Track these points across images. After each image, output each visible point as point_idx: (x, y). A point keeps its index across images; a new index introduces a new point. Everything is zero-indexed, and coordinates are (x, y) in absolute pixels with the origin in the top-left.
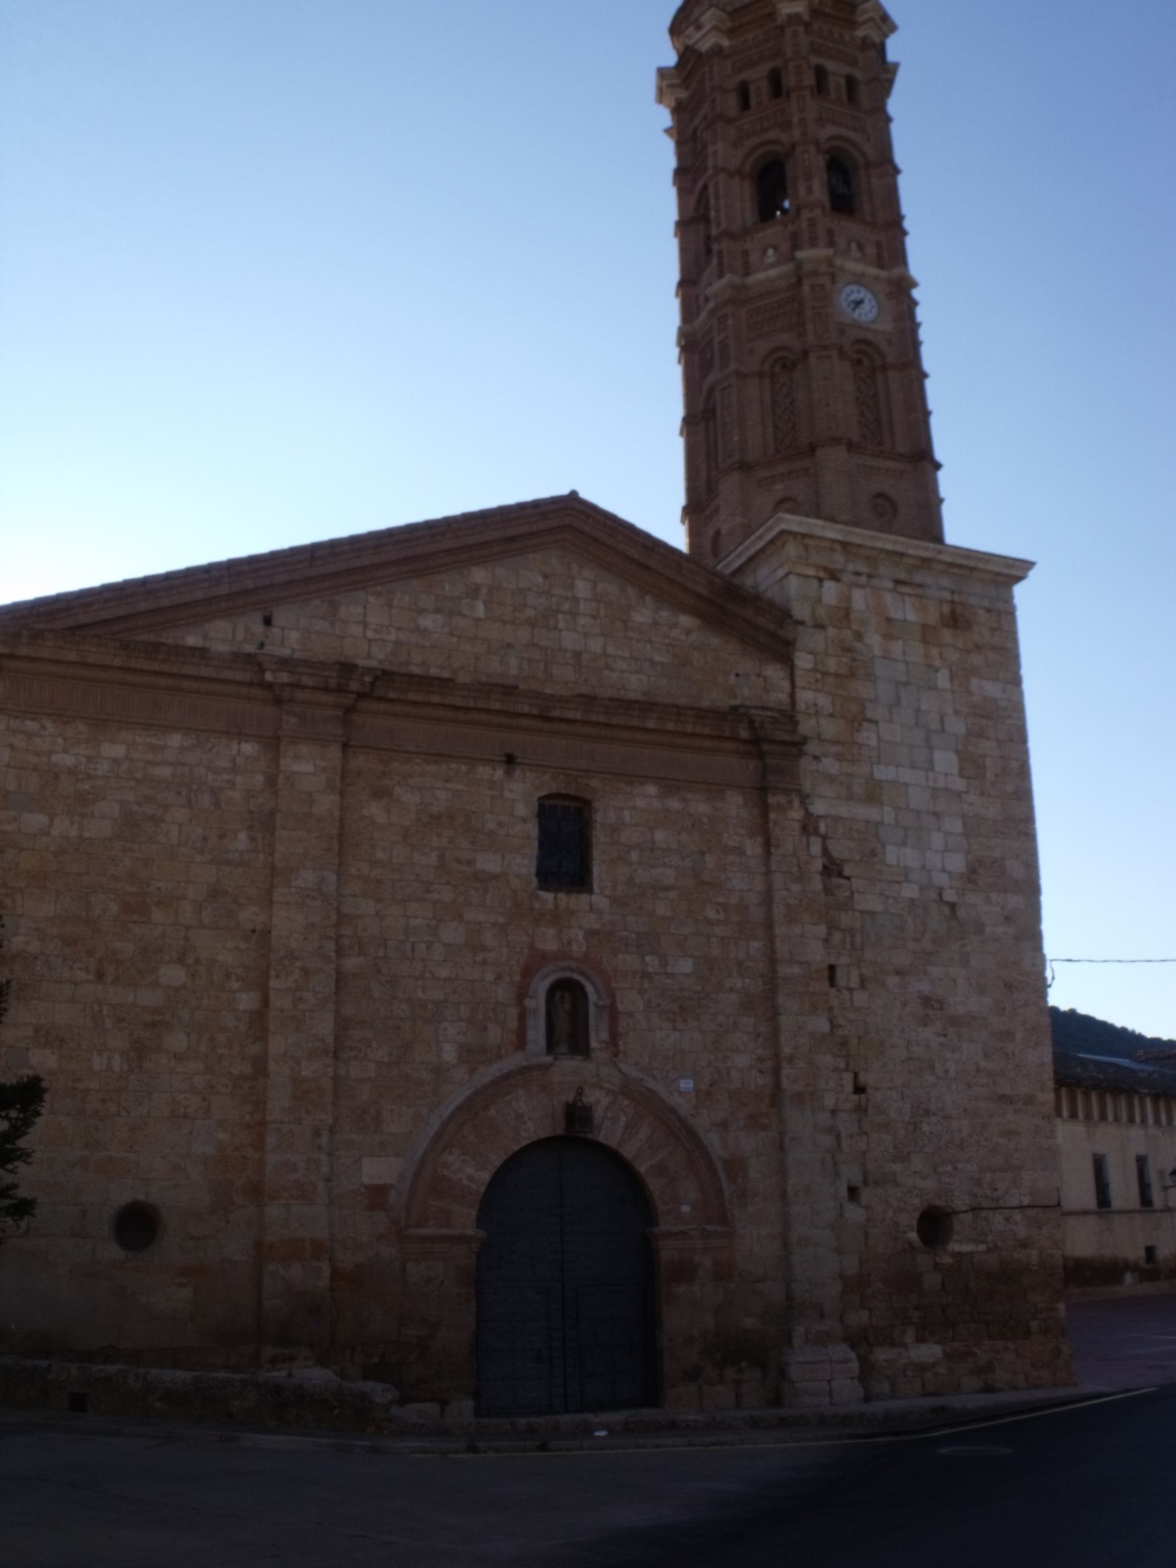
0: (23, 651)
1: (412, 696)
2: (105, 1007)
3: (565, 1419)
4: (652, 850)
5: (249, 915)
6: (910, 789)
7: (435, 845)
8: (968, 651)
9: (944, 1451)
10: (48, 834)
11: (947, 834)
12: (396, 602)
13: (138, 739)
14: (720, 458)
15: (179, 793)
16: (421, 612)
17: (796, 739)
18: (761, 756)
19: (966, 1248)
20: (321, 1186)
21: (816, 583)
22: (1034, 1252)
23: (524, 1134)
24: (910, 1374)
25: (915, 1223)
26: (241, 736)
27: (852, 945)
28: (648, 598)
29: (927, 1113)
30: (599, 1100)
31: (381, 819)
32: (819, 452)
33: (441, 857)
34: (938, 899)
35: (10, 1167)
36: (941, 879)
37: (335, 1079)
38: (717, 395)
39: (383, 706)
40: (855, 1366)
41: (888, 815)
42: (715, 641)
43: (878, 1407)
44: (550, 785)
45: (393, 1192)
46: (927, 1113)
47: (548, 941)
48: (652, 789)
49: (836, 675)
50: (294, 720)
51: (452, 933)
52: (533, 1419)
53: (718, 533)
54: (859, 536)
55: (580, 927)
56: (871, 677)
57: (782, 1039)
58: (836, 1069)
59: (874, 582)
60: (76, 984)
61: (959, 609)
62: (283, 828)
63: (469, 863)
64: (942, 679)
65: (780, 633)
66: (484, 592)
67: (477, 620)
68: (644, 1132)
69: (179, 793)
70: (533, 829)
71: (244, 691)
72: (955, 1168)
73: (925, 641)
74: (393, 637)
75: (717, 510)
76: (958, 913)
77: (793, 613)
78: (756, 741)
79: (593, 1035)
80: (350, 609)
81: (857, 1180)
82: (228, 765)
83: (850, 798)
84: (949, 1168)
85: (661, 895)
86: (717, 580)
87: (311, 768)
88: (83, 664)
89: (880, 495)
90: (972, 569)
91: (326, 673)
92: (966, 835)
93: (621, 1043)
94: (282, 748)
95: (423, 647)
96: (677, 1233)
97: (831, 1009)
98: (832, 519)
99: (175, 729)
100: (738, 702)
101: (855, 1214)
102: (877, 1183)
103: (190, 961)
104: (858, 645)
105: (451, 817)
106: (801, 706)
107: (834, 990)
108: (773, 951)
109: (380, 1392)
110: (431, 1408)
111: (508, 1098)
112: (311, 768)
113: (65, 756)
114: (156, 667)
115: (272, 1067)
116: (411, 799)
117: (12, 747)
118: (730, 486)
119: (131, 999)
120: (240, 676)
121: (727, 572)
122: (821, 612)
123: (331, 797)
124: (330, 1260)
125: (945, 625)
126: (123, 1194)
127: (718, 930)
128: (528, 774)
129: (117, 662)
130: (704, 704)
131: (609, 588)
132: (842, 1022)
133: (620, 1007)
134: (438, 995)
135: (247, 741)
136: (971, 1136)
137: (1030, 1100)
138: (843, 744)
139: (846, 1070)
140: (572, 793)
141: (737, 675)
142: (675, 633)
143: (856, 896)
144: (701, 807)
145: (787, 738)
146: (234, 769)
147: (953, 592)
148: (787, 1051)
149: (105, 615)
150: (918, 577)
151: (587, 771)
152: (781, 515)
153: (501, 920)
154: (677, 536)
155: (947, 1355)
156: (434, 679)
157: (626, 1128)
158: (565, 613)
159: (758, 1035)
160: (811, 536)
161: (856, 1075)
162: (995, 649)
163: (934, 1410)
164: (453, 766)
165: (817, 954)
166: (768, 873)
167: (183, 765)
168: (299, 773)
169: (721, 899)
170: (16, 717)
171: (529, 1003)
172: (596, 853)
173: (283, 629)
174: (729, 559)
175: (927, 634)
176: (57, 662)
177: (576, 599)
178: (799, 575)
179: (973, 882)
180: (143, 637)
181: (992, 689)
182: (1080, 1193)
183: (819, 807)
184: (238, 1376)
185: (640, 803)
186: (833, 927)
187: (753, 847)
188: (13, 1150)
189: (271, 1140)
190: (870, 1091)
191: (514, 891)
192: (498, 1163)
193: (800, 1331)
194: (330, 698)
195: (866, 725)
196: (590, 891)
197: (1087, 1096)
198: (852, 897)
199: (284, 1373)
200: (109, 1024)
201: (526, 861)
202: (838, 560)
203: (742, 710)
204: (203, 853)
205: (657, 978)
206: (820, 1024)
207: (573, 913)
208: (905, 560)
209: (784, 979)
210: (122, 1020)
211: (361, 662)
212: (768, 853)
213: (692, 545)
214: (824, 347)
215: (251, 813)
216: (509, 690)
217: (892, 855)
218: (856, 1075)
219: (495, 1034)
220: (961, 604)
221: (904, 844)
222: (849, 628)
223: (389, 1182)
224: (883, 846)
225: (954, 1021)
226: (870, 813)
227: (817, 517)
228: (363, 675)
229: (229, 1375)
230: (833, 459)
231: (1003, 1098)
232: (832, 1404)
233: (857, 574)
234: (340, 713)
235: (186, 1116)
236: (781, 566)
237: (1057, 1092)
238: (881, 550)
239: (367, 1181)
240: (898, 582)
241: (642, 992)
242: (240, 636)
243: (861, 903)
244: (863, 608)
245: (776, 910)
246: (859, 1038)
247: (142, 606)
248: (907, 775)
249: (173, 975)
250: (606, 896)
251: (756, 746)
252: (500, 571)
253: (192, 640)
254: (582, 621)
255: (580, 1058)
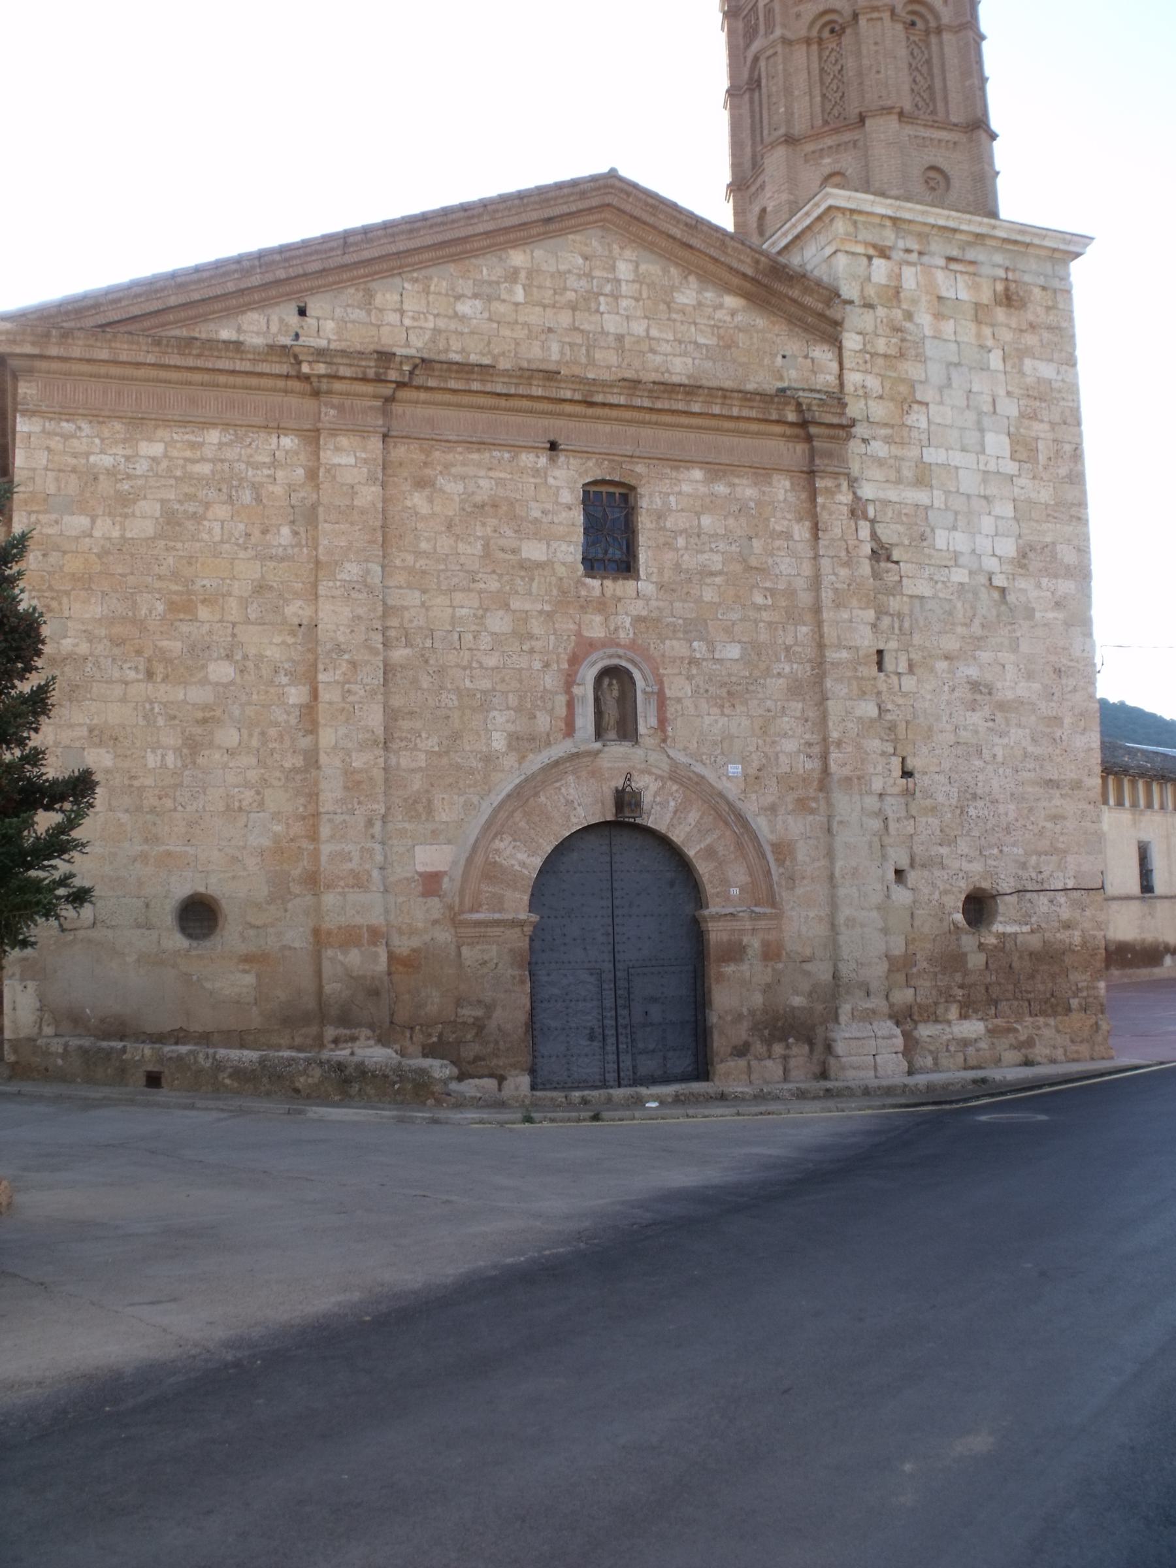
0: (54, 351)
1: (452, 384)
2: (156, 705)
3: (619, 1093)
4: (699, 536)
5: (295, 610)
6: (961, 472)
7: (479, 534)
8: (1022, 331)
9: (983, 1118)
10: (91, 536)
11: (997, 517)
12: (432, 288)
13: (175, 436)
14: (765, 132)
15: (220, 490)
16: (458, 297)
17: (844, 422)
18: (809, 439)
19: (1010, 929)
20: (375, 873)
21: (865, 260)
22: (1077, 933)
23: (574, 820)
24: (952, 1049)
25: (960, 905)
26: (280, 430)
27: (900, 629)
28: (692, 278)
29: (975, 796)
30: (648, 786)
31: (425, 509)
32: (868, 122)
33: (486, 546)
34: (987, 583)
35: (66, 857)
36: (991, 564)
37: (386, 769)
38: (762, 63)
39: (423, 396)
40: (899, 1042)
41: (939, 499)
42: (761, 322)
43: (921, 1079)
44: (595, 471)
45: (446, 879)
46: (975, 796)
47: (595, 629)
48: (697, 474)
49: (886, 356)
50: (332, 412)
51: (499, 622)
52: (586, 1093)
53: (764, 210)
54: (910, 211)
55: (626, 613)
56: (921, 358)
57: (830, 724)
58: (883, 754)
59: (925, 259)
60: (126, 683)
61: (1013, 286)
62: (326, 521)
63: (514, 552)
64: (995, 360)
65: (828, 313)
66: (523, 275)
67: (517, 304)
68: (693, 816)
69: (220, 490)
70: (578, 516)
71: (281, 384)
72: (1001, 851)
73: (978, 321)
74: (431, 325)
75: (762, 187)
76: (1008, 597)
77: (841, 292)
78: (804, 424)
79: (641, 721)
80: (386, 296)
81: (904, 863)
82: (267, 460)
83: (899, 481)
84: (995, 851)
85: (708, 581)
86: (763, 259)
87: (352, 461)
88: (116, 362)
89: (932, 168)
90: (1028, 245)
91: (363, 363)
92: (1015, 518)
93: (669, 729)
94: (322, 442)
95: (462, 334)
96: (726, 915)
97: (879, 693)
98: (883, 194)
99: (214, 425)
100: (786, 385)
101: (901, 895)
102: (923, 866)
103: (238, 657)
104: (908, 325)
105: (495, 506)
106: (849, 388)
107: (882, 674)
108: (821, 636)
109: (439, 1069)
110: (490, 1083)
111: (558, 785)
112: (352, 461)
113: (103, 456)
114: (190, 362)
115: (323, 759)
116: (454, 488)
117: (48, 449)
118: (776, 160)
119: (181, 697)
120: (277, 369)
121: (774, 250)
122: (871, 291)
123: (373, 489)
124: (387, 945)
125: (998, 303)
126: (182, 888)
127: (765, 615)
128: (572, 461)
129: (151, 359)
130: (750, 387)
131: (652, 268)
132: (889, 707)
133: (668, 693)
134: (486, 684)
135: (286, 435)
136: (1017, 820)
137: (1077, 785)
138: (892, 426)
139: (894, 754)
140: (617, 479)
141: (784, 357)
142: (719, 314)
143: (905, 580)
144: (748, 491)
145: (836, 420)
146: (274, 464)
147: (1007, 269)
148: (835, 735)
149: (136, 311)
150: (971, 255)
151: (632, 457)
152: (829, 190)
153: (547, 608)
154: (722, 215)
155: (990, 1031)
156: (474, 365)
157: (675, 812)
158: (606, 295)
159: (807, 721)
160: (860, 212)
161: (903, 759)
162: (1050, 328)
163: (975, 1082)
164: (496, 454)
165: (866, 641)
166: (816, 557)
167: (222, 461)
168: (340, 465)
169: (768, 584)
170: (51, 419)
171: (576, 690)
172: (642, 539)
173: (318, 319)
174: (774, 237)
175: (980, 313)
176: (89, 361)
177: (618, 281)
178: (847, 252)
179: (1023, 566)
180: (177, 332)
181: (1047, 371)
182: (1125, 878)
183: (867, 491)
184: (302, 1055)
185: (686, 488)
186: (881, 612)
187: (802, 532)
188: (68, 841)
189: (325, 831)
190: (917, 775)
191: (561, 579)
192: (549, 849)
193: (845, 1009)
194: (369, 389)
195: (915, 407)
196: (637, 578)
197: (1133, 783)
198: (901, 581)
199: (347, 1052)
200: (161, 722)
201: (572, 549)
202: (888, 237)
203: (788, 393)
204: (246, 549)
205: (704, 663)
206: (869, 709)
207: (620, 599)
208: (958, 236)
209: (832, 664)
210: (174, 718)
211: (399, 351)
212: (816, 538)
213: (736, 225)
214: (875, 9)
215: (293, 507)
216: (551, 376)
217: (941, 539)
218: (903, 759)
219: (543, 722)
220: (1015, 282)
221: (954, 528)
222: (899, 307)
223: (442, 869)
224: (933, 530)
225: (1002, 706)
226: (920, 496)
227: (867, 192)
228: (401, 363)
229: (294, 1054)
230: (883, 129)
231: (1050, 783)
232: (876, 1077)
233: (908, 251)
234: (379, 403)
235: (240, 809)
236: (829, 243)
237: (1104, 780)
238: (933, 226)
239: (420, 868)
240: (950, 259)
241: (689, 678)
242: (274, 328)
243: (909, 587)
244: (914, 286)
245: (824, 595)
246: (907, 722)
247: (173, 301)
248: (957, 458)
249: (221, 671)
250: (653, 583)
251: (804, 426)
252: (539, 253)
253: (226, 334)
254: (624, 303)
255: (630, 744)
